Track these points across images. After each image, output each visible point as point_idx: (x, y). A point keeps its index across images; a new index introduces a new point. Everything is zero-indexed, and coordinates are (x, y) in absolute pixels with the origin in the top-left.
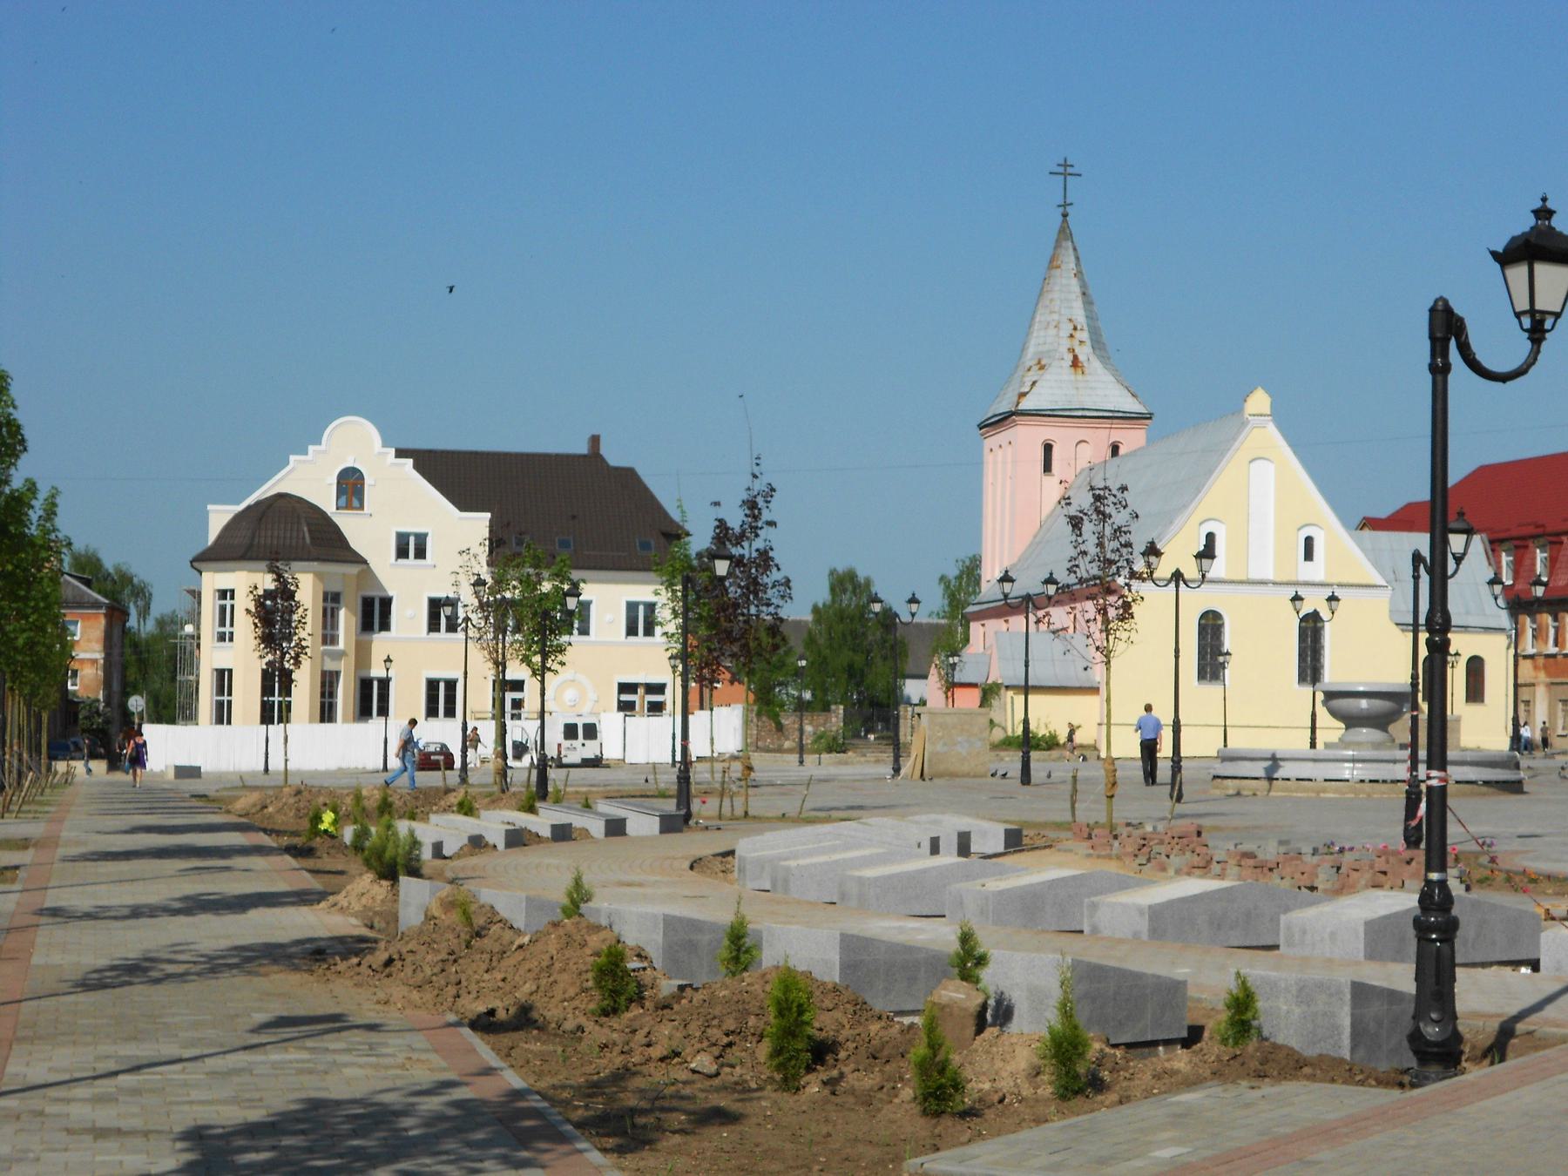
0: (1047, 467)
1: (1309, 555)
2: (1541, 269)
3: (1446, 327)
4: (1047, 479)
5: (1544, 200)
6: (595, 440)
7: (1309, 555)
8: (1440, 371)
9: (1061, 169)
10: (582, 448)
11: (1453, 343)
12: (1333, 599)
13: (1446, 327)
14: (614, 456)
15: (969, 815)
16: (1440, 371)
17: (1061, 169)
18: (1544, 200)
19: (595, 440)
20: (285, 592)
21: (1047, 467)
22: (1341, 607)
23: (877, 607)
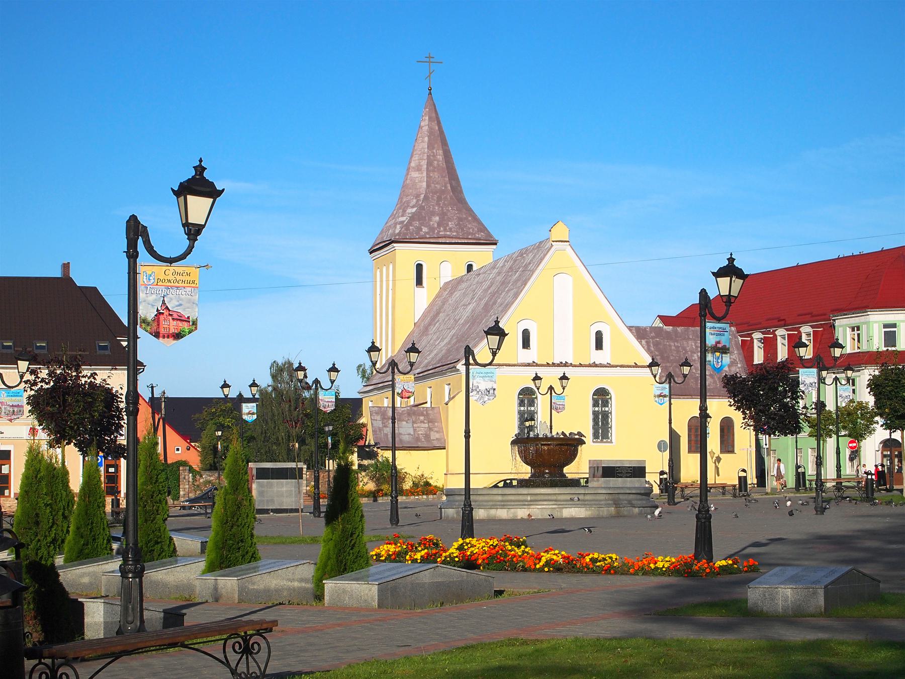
0: (419, 282)
1: (599, 345)
2: (191, 198)
3: (135, 230)
4: (419, 290)
5: (201, 161)
6: (66, 267)
7: (599, 345)
8: (132, 255)
9: (428, 60)
10: (58, 274)
11: (140, 241)
12: (564, 378)
13: (135, 230)
14: (81, 279)
15: (165, 585)
16: (132, 255)
17: (428, 60)
18: (201, 161)
19: (66, 267)
20: (704, 415)
21: (419, 282)
22: (570, 384)
23: (249, 411)
